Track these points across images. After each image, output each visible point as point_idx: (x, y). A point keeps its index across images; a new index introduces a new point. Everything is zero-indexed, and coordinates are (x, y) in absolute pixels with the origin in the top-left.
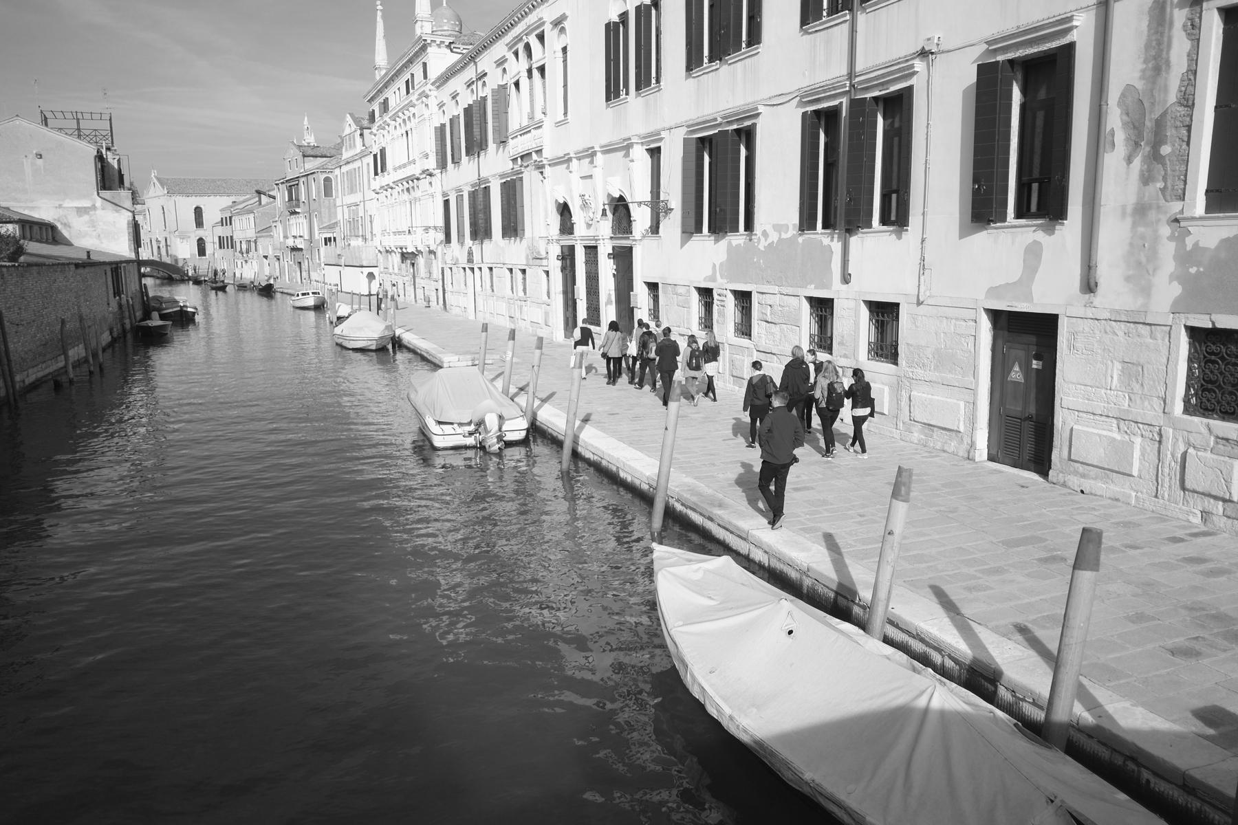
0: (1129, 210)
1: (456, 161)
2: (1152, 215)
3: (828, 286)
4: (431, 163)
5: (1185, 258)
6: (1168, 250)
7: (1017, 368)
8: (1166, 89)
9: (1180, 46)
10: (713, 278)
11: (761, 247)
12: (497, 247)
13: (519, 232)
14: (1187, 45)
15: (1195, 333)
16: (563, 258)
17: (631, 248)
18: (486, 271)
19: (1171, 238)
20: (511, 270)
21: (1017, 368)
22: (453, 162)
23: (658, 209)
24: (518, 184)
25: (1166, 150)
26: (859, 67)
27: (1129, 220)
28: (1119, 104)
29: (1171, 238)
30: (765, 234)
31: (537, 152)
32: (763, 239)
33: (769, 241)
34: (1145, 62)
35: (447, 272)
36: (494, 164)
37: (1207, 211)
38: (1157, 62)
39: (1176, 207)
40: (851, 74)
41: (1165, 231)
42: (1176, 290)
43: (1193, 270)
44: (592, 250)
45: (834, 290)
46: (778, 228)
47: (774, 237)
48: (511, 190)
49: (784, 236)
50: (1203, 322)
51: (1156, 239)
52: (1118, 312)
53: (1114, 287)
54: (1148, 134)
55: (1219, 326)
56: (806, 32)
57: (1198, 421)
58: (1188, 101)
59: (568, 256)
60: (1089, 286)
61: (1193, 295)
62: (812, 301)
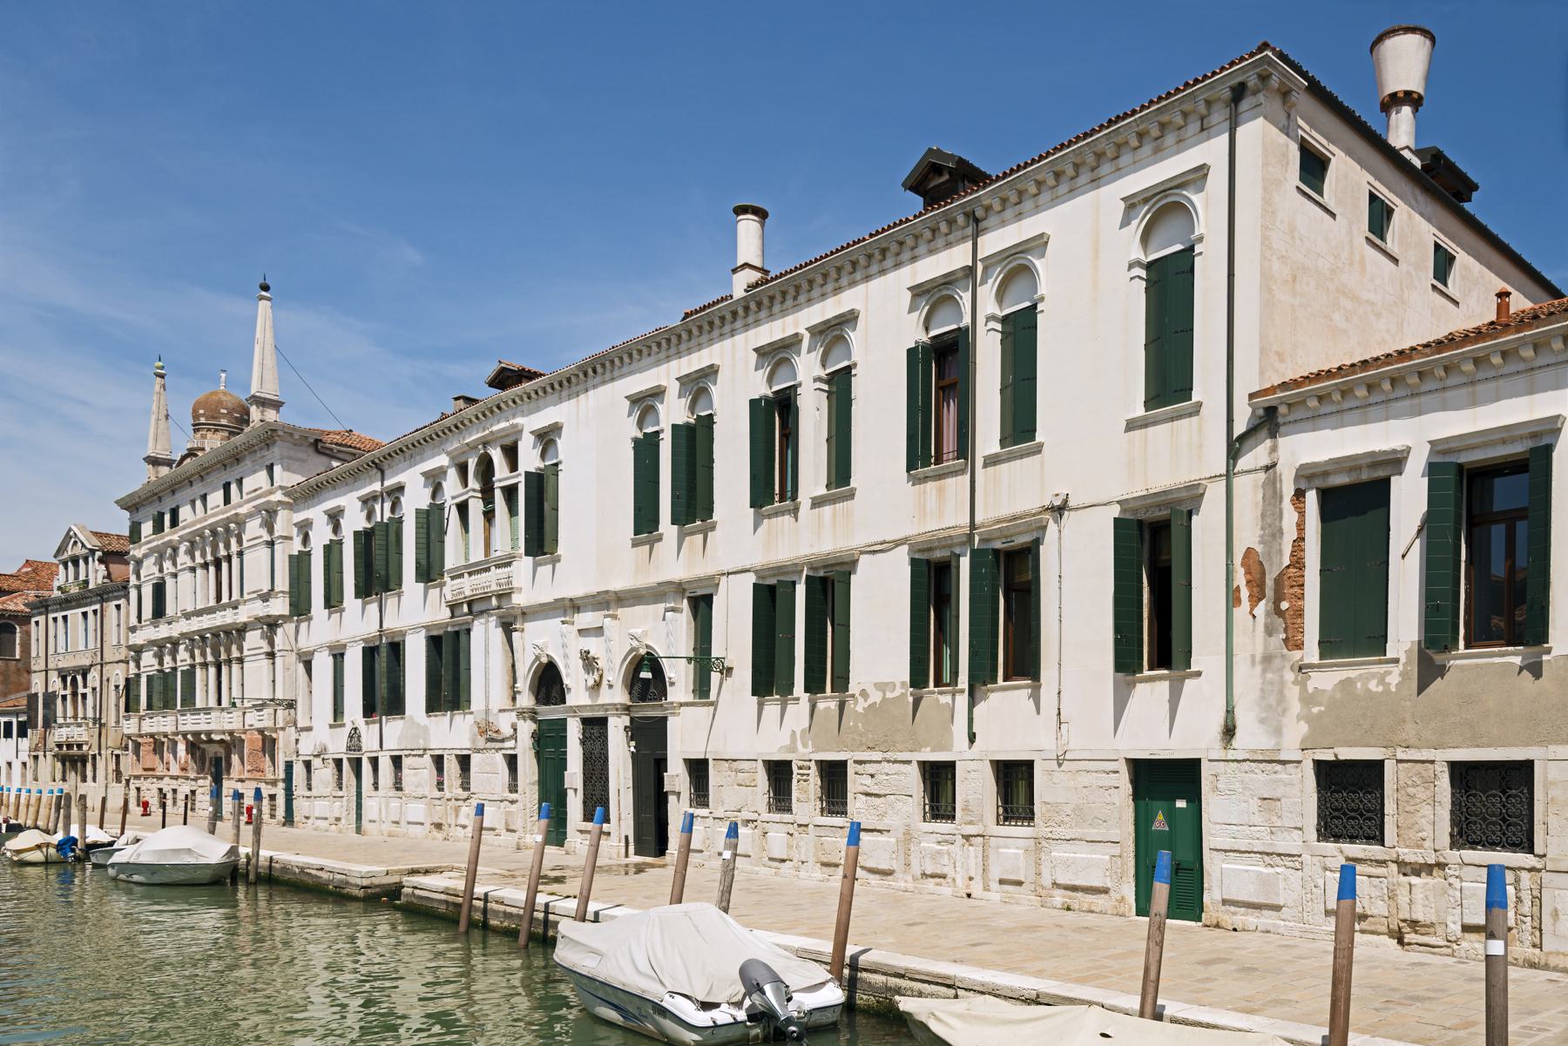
0: (1258, 659)
1: (333, 601)
2: (1277, 662)
3: (948, 748)
4: (280, 606)
5: (1308, 699)
6: (1293, 693)
7: (1160, 817)
8: (1280, 552)
9: (1290, 517)
10: (793, 749)
11: (860, 709)
12: (418, 726)
13: (463, 703)
14: (1295, 516)
15: (1319, 765)
16: (539, 739)
17: (665, 719)
18: (385, 765)
19: (1295, 682)
20: (439, 761)
21: (1160, 817)
22: (328, 604)
23: (704, 662)
24: (463, 638)
25: (1284, 605)
26: (978, 520)
27: (1258, 668)
28: (1243, 565)
29: (1295, 682)
30: (864, 693)
31: (499, 597)
32: (861, 700)
33: (870, 701)
34: (1262, 528)
35: (299, 770)
36: (414, 611)
37: (1149, 404)
38: (1272, 533)
39: (1297, 654)
40: (973, 525)
41: (1290, 676)
42: (1304, 728)
43: (1315, 710)
44: (595, 727)
45: (956, 750)
46: (881, 687)
47: (876, 697)
48: (448, 651)
49: (889, 695)
50: (1328, 756)
51: (1282, 683)
52: (1254, 751)
53: (1250, 737)
54: (1269, 592)
55: (1341, 757)
56: (916, 481)
57: (1330, 847)
58: (1298, 563)
59: (549, 741)
60: (1229, 731)
61: (1319, 731)
62: (924, 766)
